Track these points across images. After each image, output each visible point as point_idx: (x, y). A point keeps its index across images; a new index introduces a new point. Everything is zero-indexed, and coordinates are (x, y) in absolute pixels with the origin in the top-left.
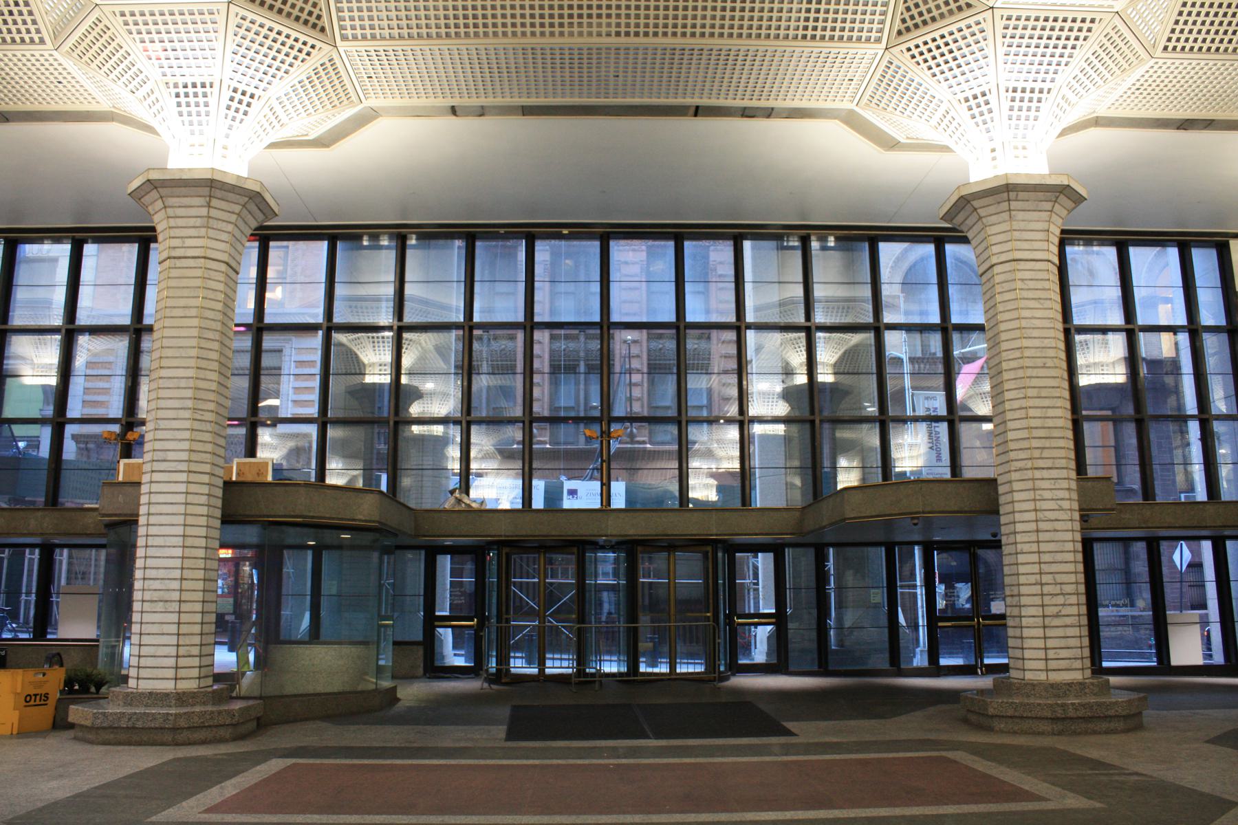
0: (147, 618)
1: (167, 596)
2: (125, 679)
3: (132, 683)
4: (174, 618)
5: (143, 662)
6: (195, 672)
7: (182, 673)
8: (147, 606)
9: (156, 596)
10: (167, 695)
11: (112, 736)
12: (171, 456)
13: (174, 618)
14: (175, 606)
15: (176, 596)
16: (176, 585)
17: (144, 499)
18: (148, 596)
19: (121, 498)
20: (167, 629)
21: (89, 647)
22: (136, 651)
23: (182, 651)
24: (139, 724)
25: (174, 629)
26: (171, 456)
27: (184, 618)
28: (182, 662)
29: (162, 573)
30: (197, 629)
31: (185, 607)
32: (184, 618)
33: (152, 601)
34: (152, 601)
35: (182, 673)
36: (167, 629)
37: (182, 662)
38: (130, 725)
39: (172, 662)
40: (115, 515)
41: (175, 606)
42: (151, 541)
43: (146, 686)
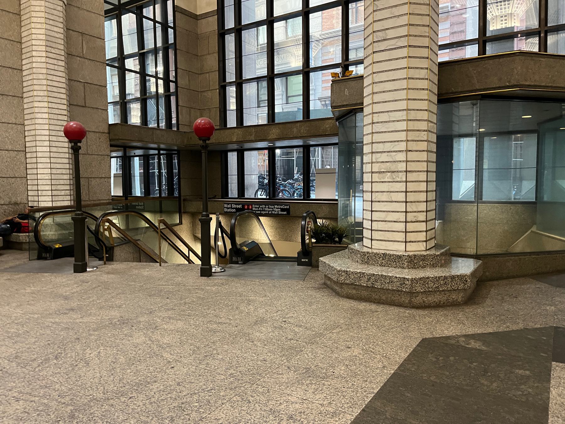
0: (376, 187)
1: (393, 167)
2: (361, 240)
3: (366, 242)
4: (402, 187)
5: (376, 216)
6: (422, 236)
7: (411, 237)
8: (376, 177)
9: (383, 167)
10: (400, 257)
11: (354, 292)
12: (391, 34)
13: (402, 187)
14: (402, 177)
15: (402, 167)
16: (401, 157)
17: (366, 92)
18: (376, 168)
19: (347, 92)
20: (395, 197)
21: (332, 204)
22: (368, 206)
23: (410, 217)
24: (378, 285)
25: (401, 237)
26: (391, 34)
27: (411, 187)
28: (410, 227)
29: (388, 147)
30: (423, 197)
31: (411, 177)
32: (411, 187)
33: (380, 172)
34: (380, 172)
35: (411, 237)
36: (395, 197)
37: (410, 227)
38: (369, 284)
39: (401, 227)
40: (343, 106)
41: (402, 177)
42: (376, 235)
43: (379, 247)
